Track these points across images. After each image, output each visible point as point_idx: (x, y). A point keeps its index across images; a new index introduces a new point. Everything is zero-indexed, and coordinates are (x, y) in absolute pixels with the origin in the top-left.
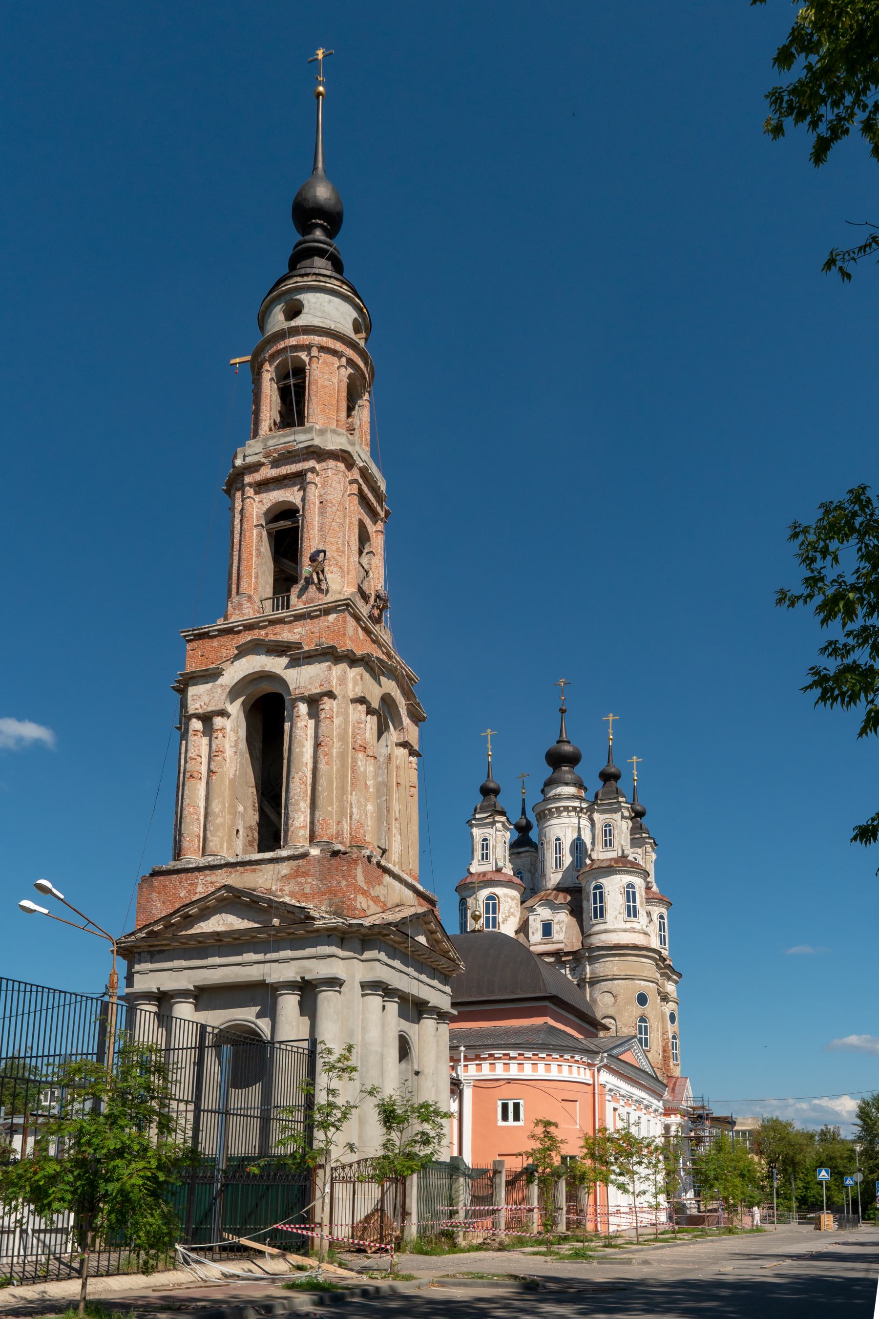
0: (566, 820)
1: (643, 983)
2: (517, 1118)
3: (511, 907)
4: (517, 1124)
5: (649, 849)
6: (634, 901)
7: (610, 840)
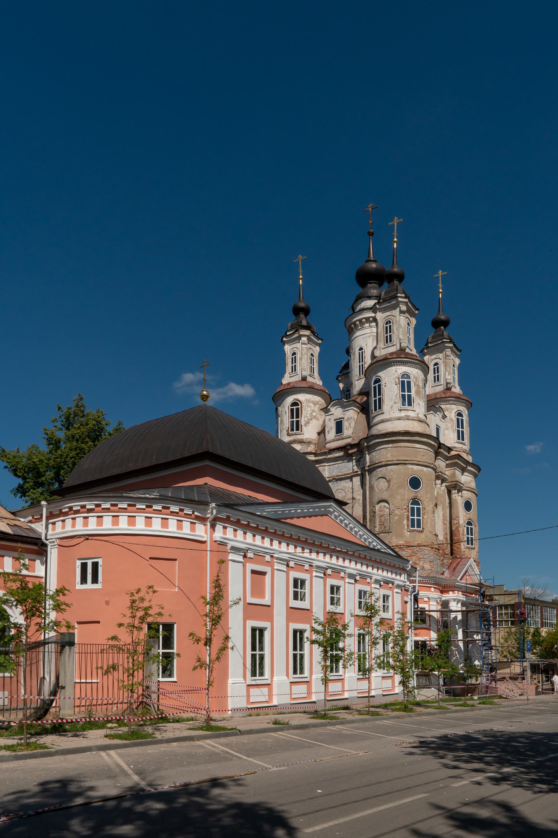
0: (368, 331)
1: (415, 467)
2: (95, 580)
3: (313, 411)
4: (95, 586)
5: (448, 352)
6: (409, 390)
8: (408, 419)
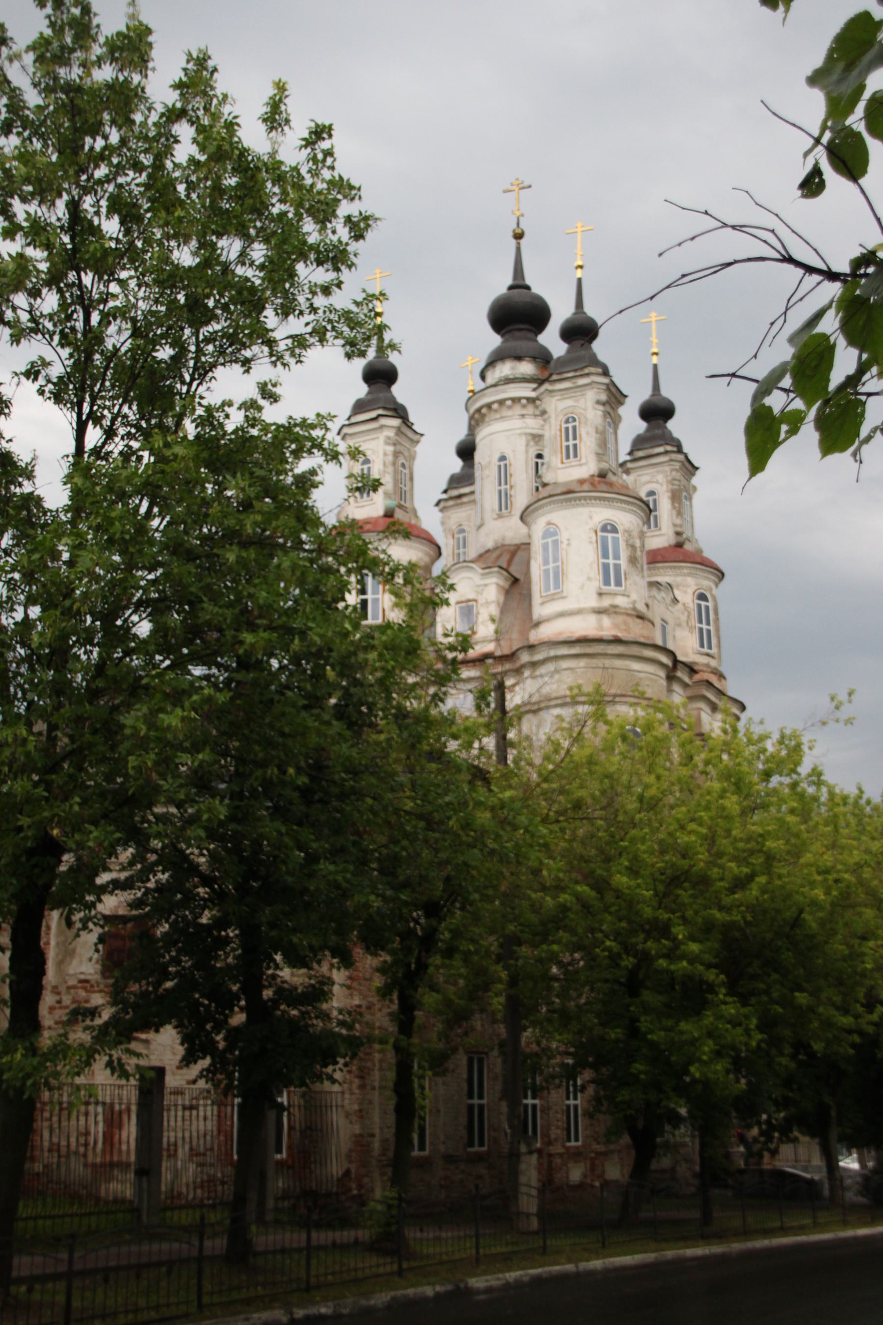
7: (575, 446)
8: (616, 613)
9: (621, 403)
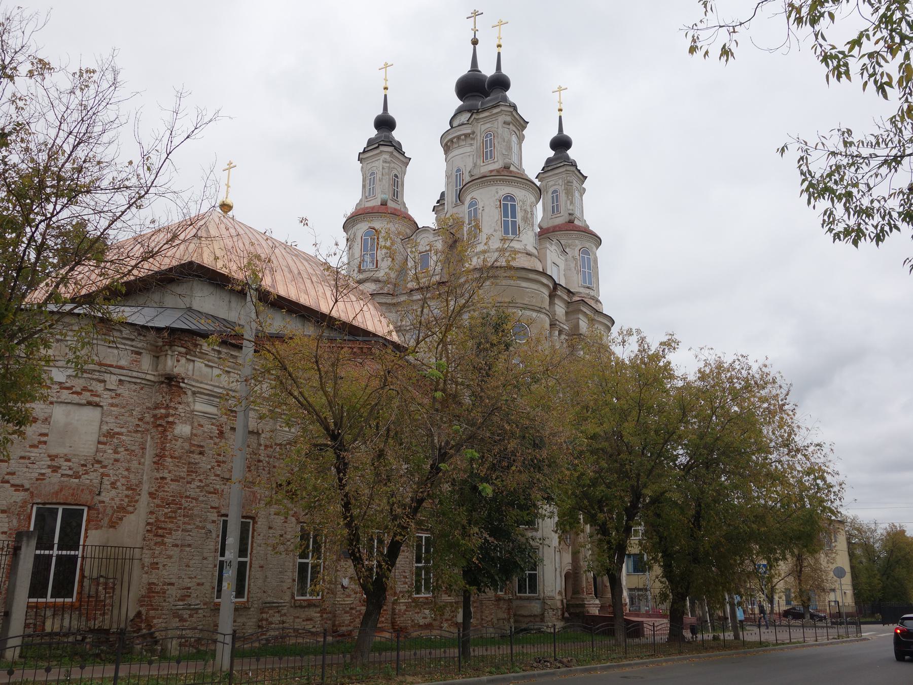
9: (524, 128)
